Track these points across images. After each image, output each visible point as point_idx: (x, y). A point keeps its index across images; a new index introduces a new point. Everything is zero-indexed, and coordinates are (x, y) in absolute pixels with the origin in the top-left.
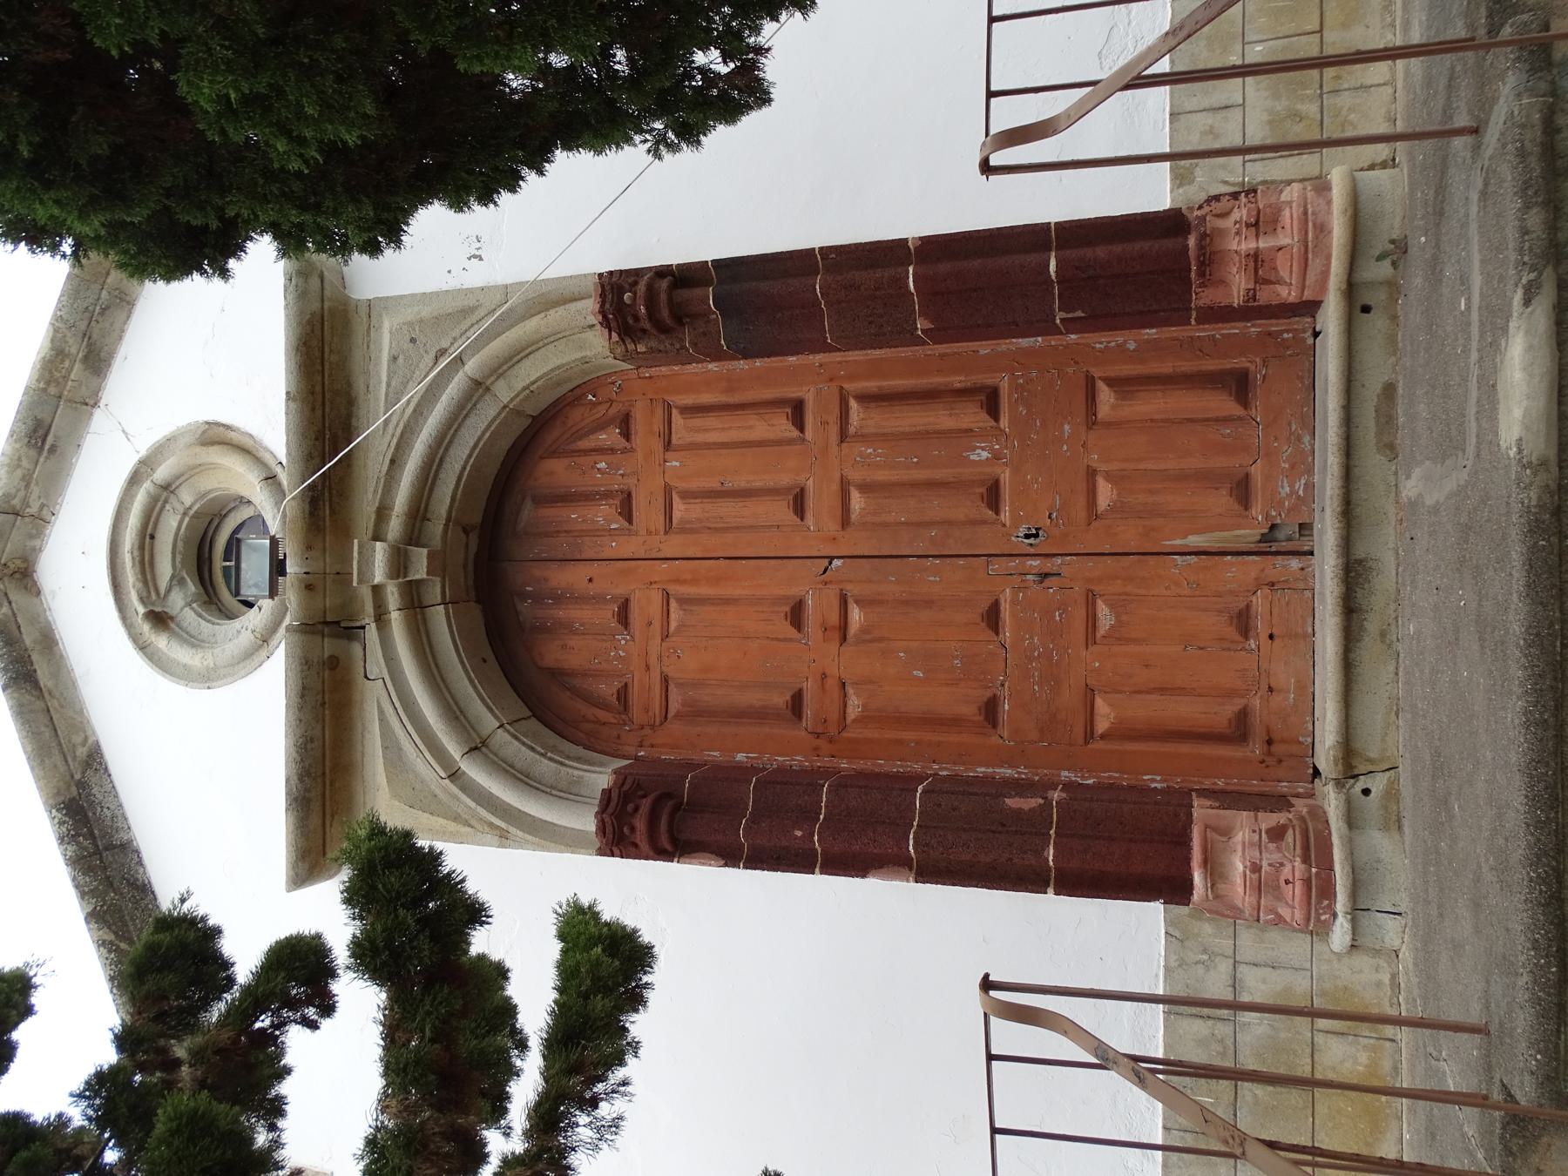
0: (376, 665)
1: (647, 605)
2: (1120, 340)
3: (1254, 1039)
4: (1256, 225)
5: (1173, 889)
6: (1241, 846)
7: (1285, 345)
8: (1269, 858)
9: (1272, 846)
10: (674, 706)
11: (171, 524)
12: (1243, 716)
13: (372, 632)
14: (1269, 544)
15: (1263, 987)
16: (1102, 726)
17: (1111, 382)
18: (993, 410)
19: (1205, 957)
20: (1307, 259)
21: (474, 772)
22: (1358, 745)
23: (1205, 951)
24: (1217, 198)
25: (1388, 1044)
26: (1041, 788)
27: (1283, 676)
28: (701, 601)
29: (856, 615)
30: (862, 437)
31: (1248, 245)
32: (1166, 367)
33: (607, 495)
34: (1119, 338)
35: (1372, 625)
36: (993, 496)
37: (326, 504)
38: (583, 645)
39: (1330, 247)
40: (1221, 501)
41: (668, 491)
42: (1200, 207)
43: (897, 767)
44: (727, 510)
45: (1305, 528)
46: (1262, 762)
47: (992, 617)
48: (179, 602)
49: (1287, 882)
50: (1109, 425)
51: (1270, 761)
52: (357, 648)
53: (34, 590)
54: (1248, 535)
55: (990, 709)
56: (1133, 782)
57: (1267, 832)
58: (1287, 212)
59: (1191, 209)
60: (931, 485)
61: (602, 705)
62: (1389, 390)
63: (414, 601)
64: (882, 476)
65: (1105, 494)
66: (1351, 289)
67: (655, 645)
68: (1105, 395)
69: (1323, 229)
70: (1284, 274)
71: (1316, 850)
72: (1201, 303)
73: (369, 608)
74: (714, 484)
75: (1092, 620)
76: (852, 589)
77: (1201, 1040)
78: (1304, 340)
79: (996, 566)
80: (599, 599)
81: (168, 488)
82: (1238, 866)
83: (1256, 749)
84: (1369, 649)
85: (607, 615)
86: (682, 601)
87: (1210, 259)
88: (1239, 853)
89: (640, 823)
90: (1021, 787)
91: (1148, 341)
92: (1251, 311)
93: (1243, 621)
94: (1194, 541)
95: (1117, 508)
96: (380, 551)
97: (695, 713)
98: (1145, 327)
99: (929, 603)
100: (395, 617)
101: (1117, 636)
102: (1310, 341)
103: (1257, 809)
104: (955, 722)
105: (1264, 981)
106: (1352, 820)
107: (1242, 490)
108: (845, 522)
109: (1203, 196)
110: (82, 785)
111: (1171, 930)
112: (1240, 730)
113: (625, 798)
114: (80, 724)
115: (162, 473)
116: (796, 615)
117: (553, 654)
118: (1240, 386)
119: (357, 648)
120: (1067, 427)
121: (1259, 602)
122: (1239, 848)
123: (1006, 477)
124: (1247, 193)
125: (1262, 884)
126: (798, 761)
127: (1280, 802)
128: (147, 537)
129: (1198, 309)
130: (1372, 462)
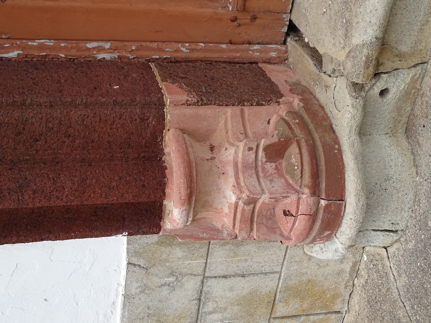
5: (137, 215)
9: (270, 167)
15: (229, 294)
19: (171, 279)
22: (392, 38)
23: (172, 274)
25: (334, 316)
46: (234, 20)
49: (286, 213)
51: (245, 18)
56: (73, 53)
57: (265, 149)
88: (232, 180)
103: (241, 102)
105: (231, 289)
111: (134, 260)
122: (230, 171)
127: (265, 92)
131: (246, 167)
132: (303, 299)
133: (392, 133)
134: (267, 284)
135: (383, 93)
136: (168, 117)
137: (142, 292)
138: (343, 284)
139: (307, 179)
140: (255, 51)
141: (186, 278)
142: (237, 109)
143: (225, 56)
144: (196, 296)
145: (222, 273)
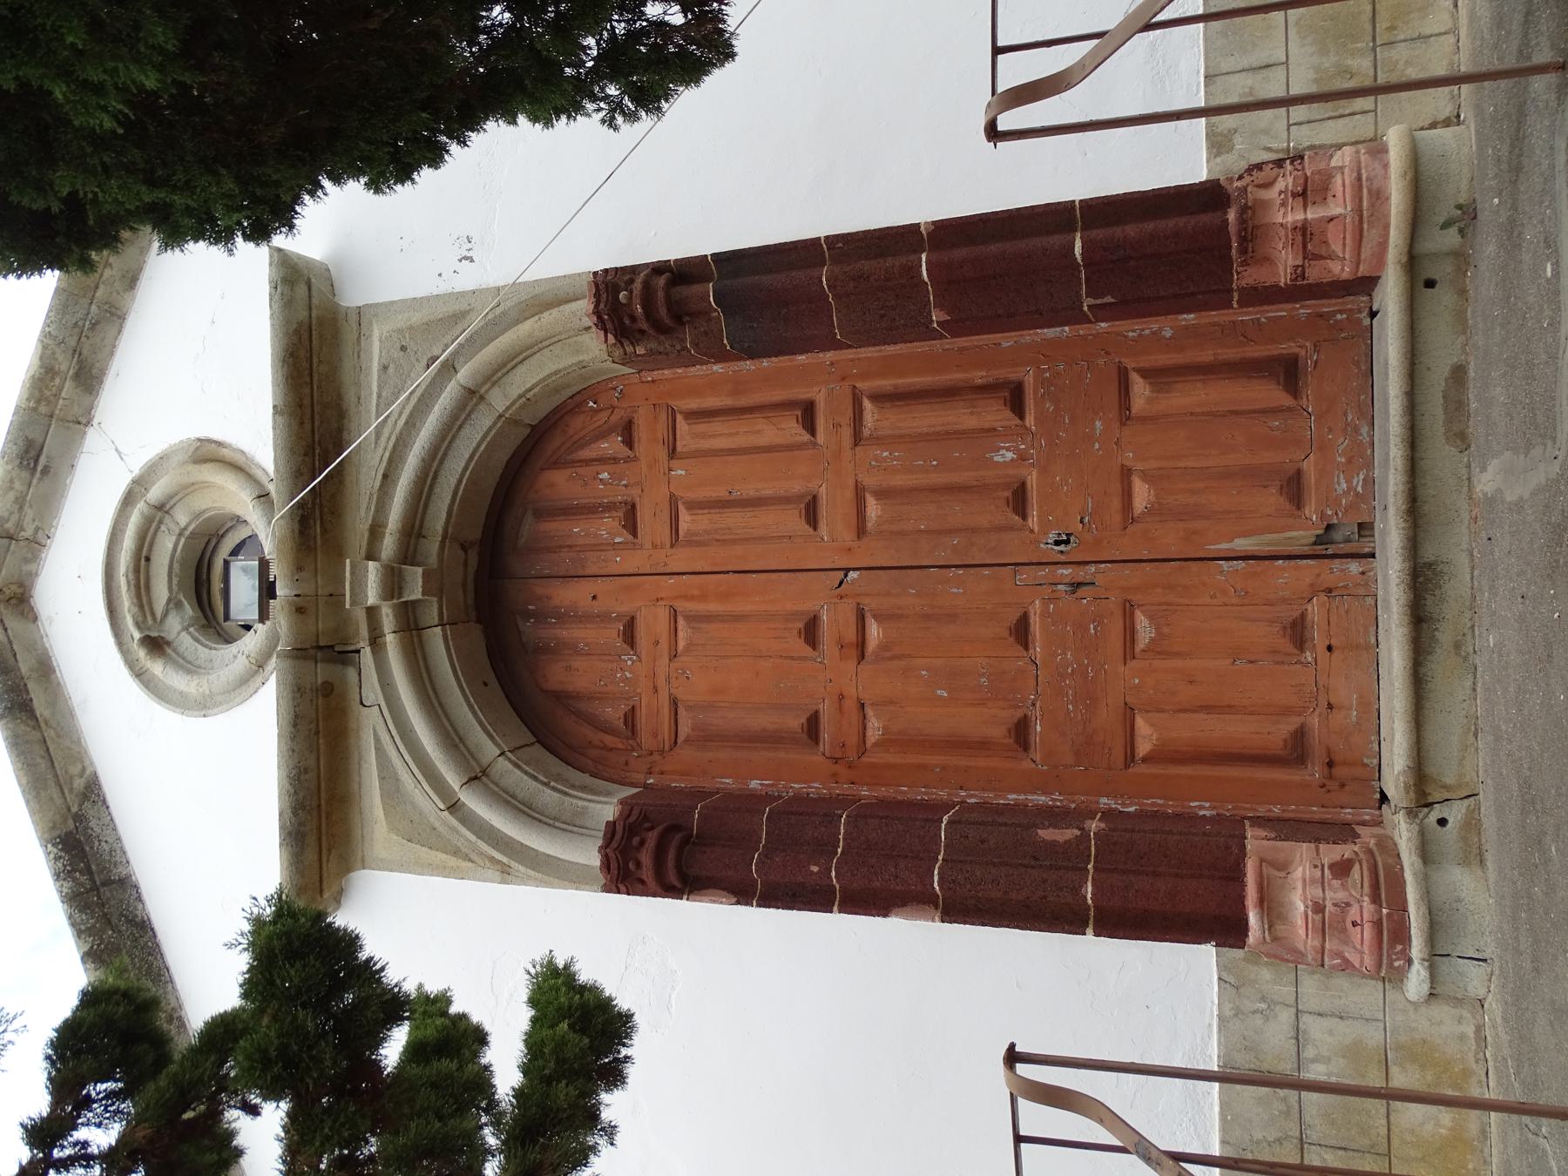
0: (372, 690)
1: (654, 622)
2: (1155, 327)
4: (1304, 194)
5: (1224, 928)
6: (1302, 879)
7: (1339, 327)
8: (1335, 894)
9: (1337, 883)
10: (685, 729)
11: (166, 545)
12: (1300, 735)
13: (367, 655)
14: (1325, 546)
15: (1329, 1040)
16: (1143, 748)
17: (1145, 373)
18: (1018, 407)
19: (1264, 1006)
20: (1361, 230)
22: (1431, 770)
23: (1263, 999)
24: (1259, 167)
28: (708, 618)
29: (874, 631)
30: (878, 440)
31: (1295, 216)
32: (1206, 356)
33: (610, 507)
34: (1153, 324)
35: (1445, 636)
36: (1019, 500)
38: (589, 667)
39: (1388, 216)
40: (1271, 499)
41: (673, 501)
42: (1241, 177)
44: (735, 520)
45: (1365, 528)
46: (1323, 786)
47: (1021, 631)
48: (175, 627)
49: (1354, 924)
50: (1143, 420)
51: (1334, 785)
52: (351, 673)
54: (1301, 536)
55: (1021, 731)
56: (1179, 810)
57: (1331, 867)
58: (1338, 180)
59: (1230, 180)
60: (951, 489)
61: (612, 732)
62: (1459, 374)
64: (899, 481)
65: (1142, 495)
66: (1412, 262)
68: (1140, 389)
69: (1379, 196)
70: (1336, 248)
71: (1386, 888)
72: (1243, 283)
73: (364, 631)
74: (720, 493)
75: (1130, 632)
76: (869, 603)
78: (1359, 321)
79: (1024, 576)
80: (604, 618)
81: (162, 508)
82: (1298, 904)
83: (1315, 772)
84: (1440, 664)
85: (611, 635)
86: (692, 619)
87: (1252, 234)
88: (1300, 891)
90: (1055, 816)
91: (1186, 328)
92: (1300, 290)
93: (1298, 632)
94: (1242, 544)
97: (705, 738)
98: (1182, 313)
99: (952, 617)
102: (1367, 322)
103: (1317, 840)
104: (983, 746)
105: (1331, 1033)
106: (1426, 853)
107: (1294, 488)
108: (861, 531)
109: (1244, 165)
110: (79, 818)
112: (1297, 750)
114: (77, 753)
115: (155, 493)
117: (558, 675)
118: (1289, 373)
119: (351, 673)
121: (1315, 610)
122: (1299, 885)
123: (1033, 479)
124: (1293, 160)
125: (1325, 921)
126: (816, 788)
129: (1241, 290)
131: (1313, 881)
132: (1423, 1067)
133: (1465, 862)
134: (1373, 1036)
135: (1442, 822)
136: (1249, 847)
137: (1236, 1015)
138: (1471, 1055)
139: (1366, 889)
140: (1347, 814)
141: (1278, 1008)
142: (1313, 845)
143: (1317, 817)
144: (1293, 1034)
145: (1317, 1009)
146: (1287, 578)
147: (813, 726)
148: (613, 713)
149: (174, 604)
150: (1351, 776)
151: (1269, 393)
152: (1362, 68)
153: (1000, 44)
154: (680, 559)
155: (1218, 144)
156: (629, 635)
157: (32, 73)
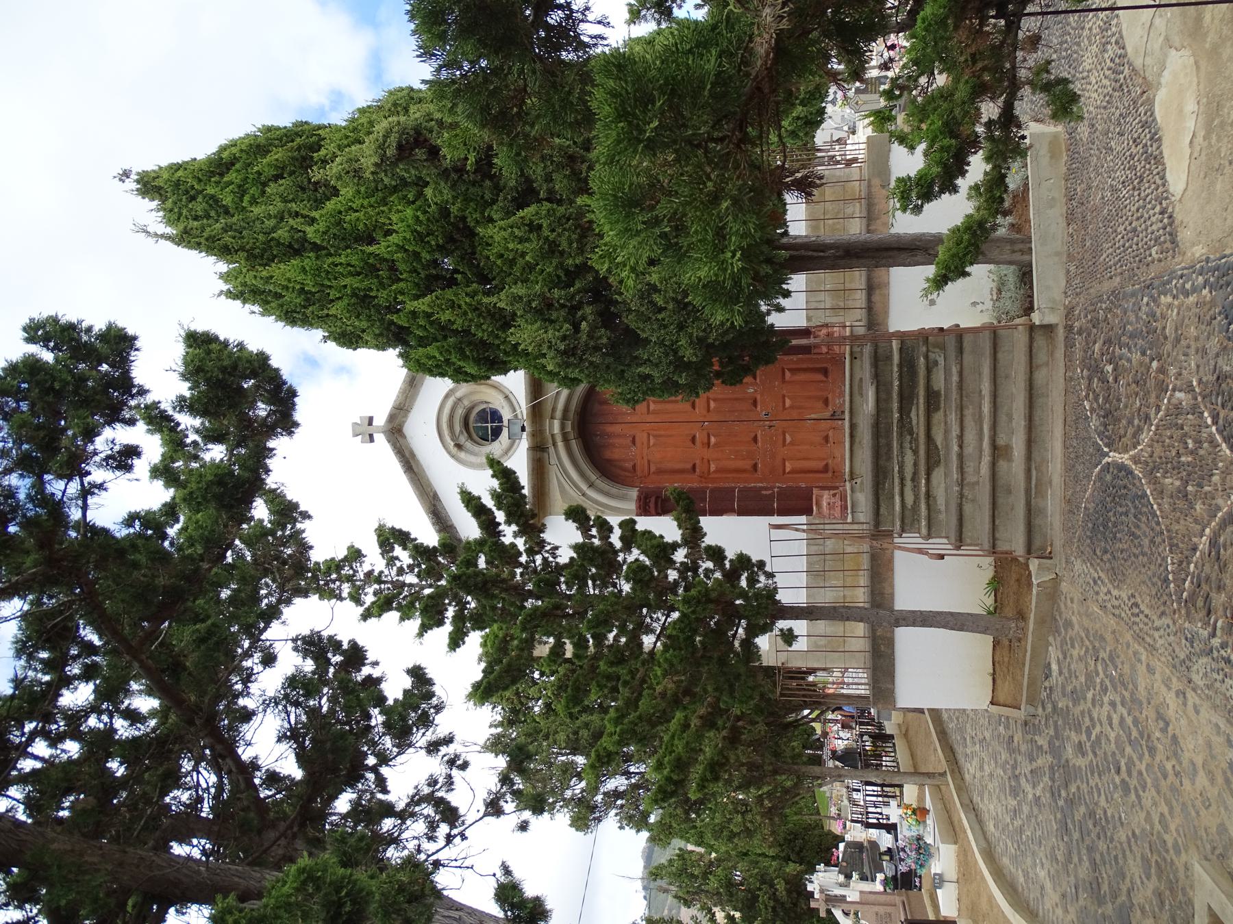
0: (554, 460)
1: (641, 437)
3: (814, 527)
5: (807, 511)
8: (833, 500)
10: (653, 469)
11: (460, 412)
12: (827, 465)
13: (552, 450)
14: (833, 417)
16: (788, 470)
21: (591, 493)
26: (772, 488)
27: (837, 454)
28: (660, 436)
29: (713, 440)
32: (804, 366)
35: (857, 440)
36: (755, 403)
37: (536, 412)
38: (617, 452)
40: (820, 404)
43: (727, 485)
45: (843, 412)
47: (755, 439)
48: (462, 439)
50: (790, 382)
52: (546, 455)
53: (404, 437)
54: (827, 414)
55: (755, 466)
61: (625, 470)
63: (566, 439)
65: (788, 403)
66: (851, 353)
67: (645, 451)
68: (788, 374)
71: (843, 498)
73: (550, 441)
77: (811, 536)
81: (459, 400)
82: (825, 504)
83: (830, 474)
84: (856, 446)
86: (655, 436)
89: (652, 505)
90: (766, 489)
93: (826, 439)
94: (813, 416)
95: (791, 407)
96: (557, 424)
97: (660, 472)
100: (560, 444)
101: (791, 444)
104: (744, 471)
106: (852, 490)
108: (709, 411)
112: (826, 469)
113: (646, 498)
114: (430, 485)
116: (693, 440)
117: (608, 454)
118: (825, 372)
120: (738, 602)
121: (831, 433)
123: (758, 397)
126: (695, 485)
128: (451, 417)
130: (857, 398)
146: (824, 425)
147: (694, 466)
148: (629, 465)
149: (461, 432)
150: (837, 474)
151: (820, 377)
152: (842, 304)
153: (905, 637)
154: (650, 418)
155: (809, 319)
156: (634, 442)
157: (323, 212)
